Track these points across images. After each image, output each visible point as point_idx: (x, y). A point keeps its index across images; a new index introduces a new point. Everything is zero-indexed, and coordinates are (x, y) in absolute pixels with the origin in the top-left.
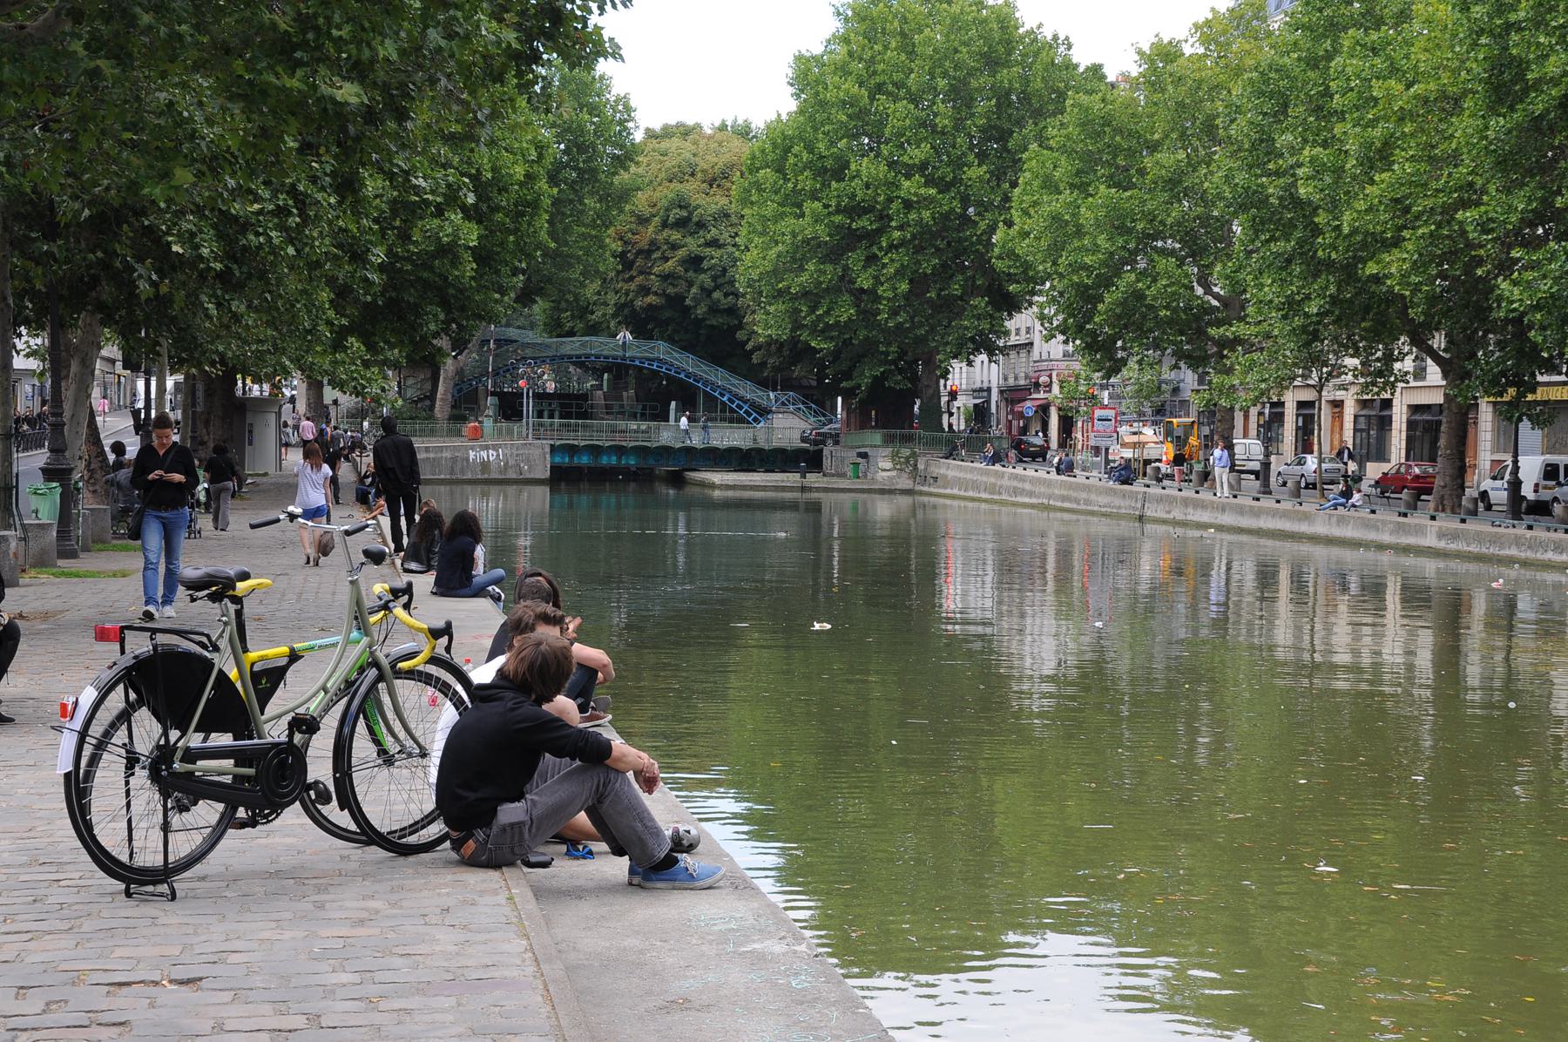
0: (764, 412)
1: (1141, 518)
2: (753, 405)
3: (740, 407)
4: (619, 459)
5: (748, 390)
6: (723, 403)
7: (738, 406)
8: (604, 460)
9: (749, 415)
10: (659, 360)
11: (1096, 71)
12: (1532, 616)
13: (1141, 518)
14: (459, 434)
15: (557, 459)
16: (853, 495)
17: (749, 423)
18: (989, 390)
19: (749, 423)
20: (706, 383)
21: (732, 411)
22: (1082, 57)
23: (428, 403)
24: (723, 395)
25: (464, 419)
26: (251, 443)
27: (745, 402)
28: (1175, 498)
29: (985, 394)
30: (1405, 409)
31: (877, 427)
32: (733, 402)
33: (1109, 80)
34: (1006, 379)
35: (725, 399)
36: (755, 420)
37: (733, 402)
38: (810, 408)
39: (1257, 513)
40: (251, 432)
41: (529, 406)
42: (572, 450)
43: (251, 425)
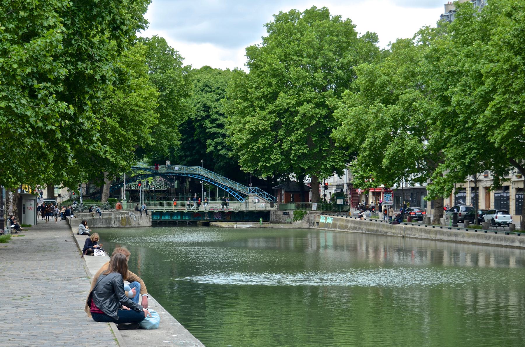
0: (244, 196)
1: (403, 237)
2: (240, 193)
3: (234, 194)
4: (161, 217)
5: (238, 187)
6: (227, 192)
7: (233, 193)
8: (175, 218)
9: (238, 197)
10: (199, 174)
11: (372, 37)
12: (483, 296)
13: (403, 237)
14: (113, 208)
15: (155, 218)
16: (293, 227)
17: (238, 201)
18: (343, 185)
19: (238, 201)
20: (219, 184)
21: (231, 196)
22: (356, 30)
23: (99, 195)
24: (226, 189)
25: (114, 202)
26: (24, 213)
27: (237, 192)
28: (417, 228)
29: (341, 187)
30: (514, 190)
31: (293, 201)
32: (231, 192)
33: (378, 45)
34: (350, 180)
35: (227, 191)
36: (241, 199)
37: (231, 192)
38: (265, 194)
39: (450, 235)
40: (24, 208)
41: (141, 195)
42: (161, 214)
43: (24, 205)
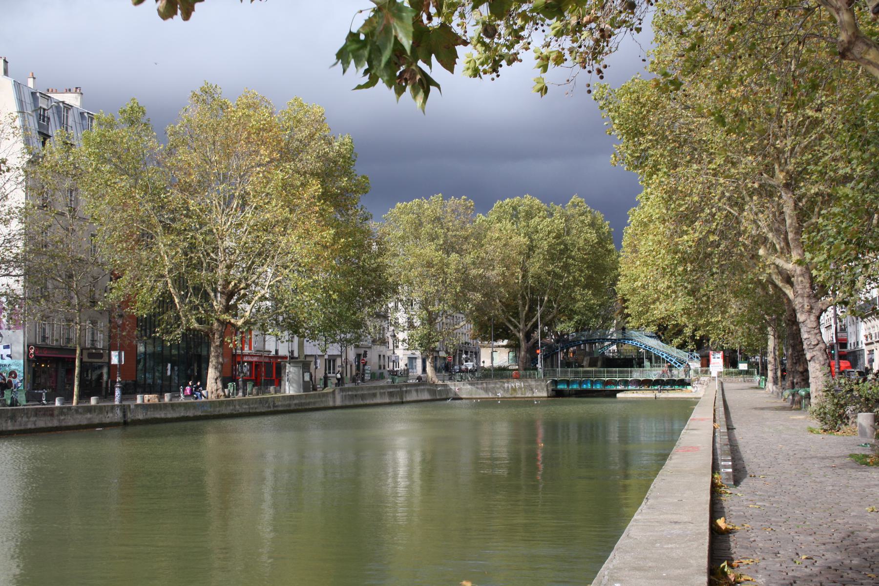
35: (664, 357)
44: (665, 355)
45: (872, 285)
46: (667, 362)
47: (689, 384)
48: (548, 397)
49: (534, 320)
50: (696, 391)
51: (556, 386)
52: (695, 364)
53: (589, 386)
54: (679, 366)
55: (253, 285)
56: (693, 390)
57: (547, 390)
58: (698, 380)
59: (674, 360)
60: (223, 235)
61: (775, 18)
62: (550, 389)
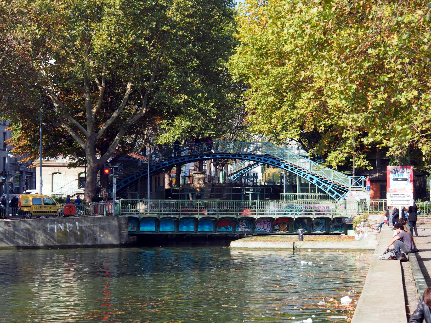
35: (314, 182)
44: (316, 179)
45: (137, 145)
46: (320, 190)
47: (350, 227)
48: (121, 246)
49: (310, 183)
50: (361, 239)
51: (139, 227)
52: (362, 193)
53: (191, 229)
54: (337, 196)
55: (36, 118)
56: (357, 237)
57: (120, 234)
58: (366, 220)
59: (330, 188)
60: (24, 95)
61: (248, 44)
62: (125, 232)
